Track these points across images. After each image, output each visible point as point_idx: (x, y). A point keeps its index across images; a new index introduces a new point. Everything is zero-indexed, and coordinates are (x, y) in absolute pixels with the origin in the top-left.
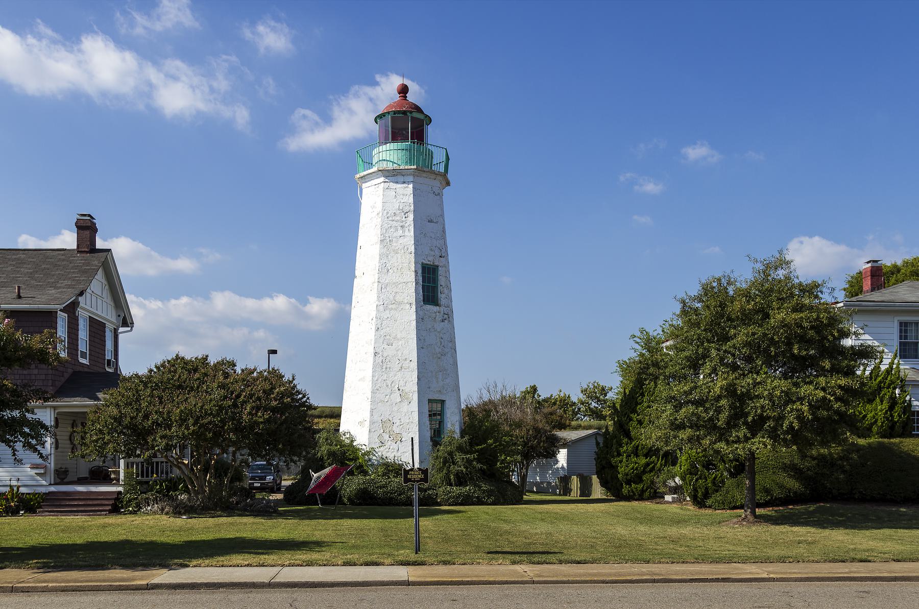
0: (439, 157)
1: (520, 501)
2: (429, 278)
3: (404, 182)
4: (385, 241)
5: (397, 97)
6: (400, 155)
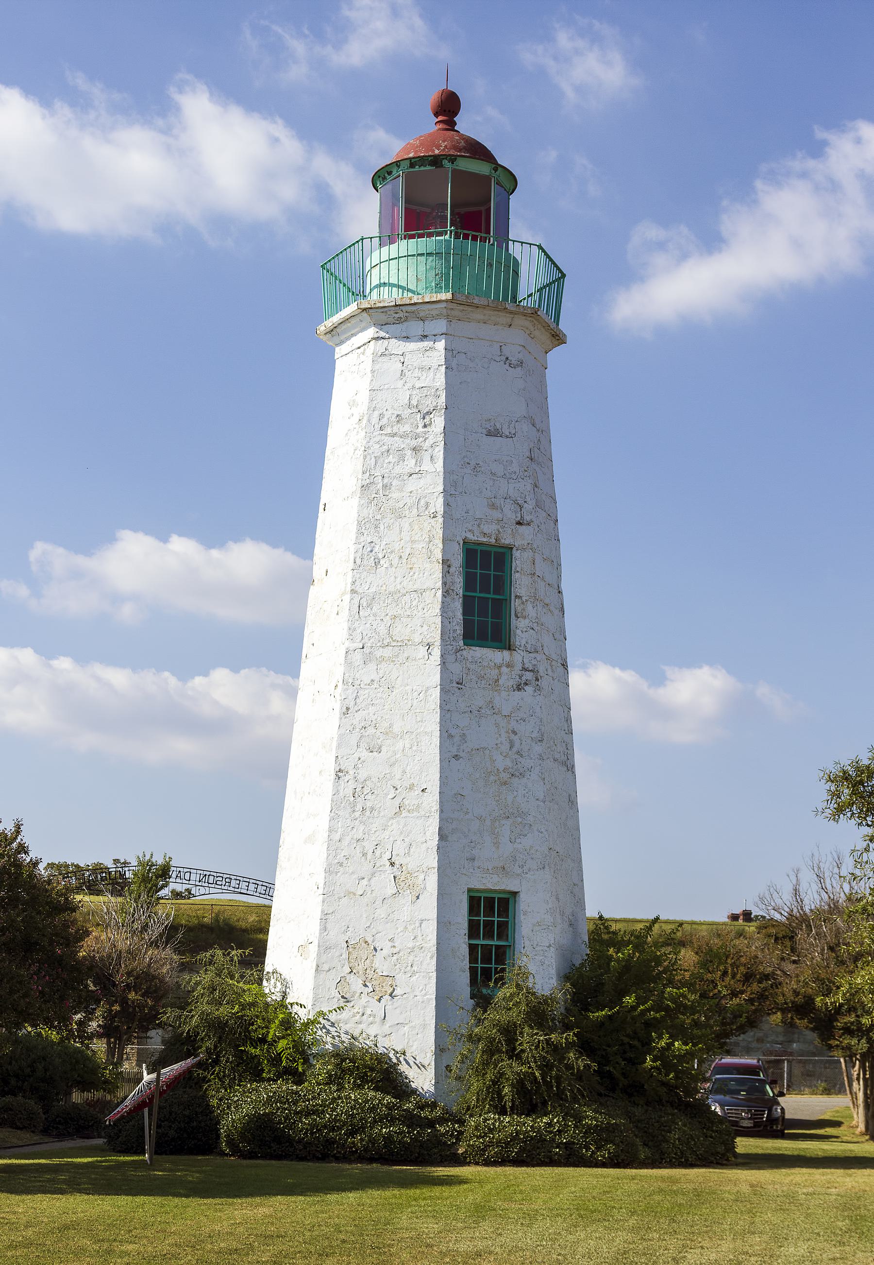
0: (531, 277)
1: (724, 1157)
2: (485, 578)
3: (424, 337)
4: (373, 488)
5: (430, 125)
6: (422, 268)
